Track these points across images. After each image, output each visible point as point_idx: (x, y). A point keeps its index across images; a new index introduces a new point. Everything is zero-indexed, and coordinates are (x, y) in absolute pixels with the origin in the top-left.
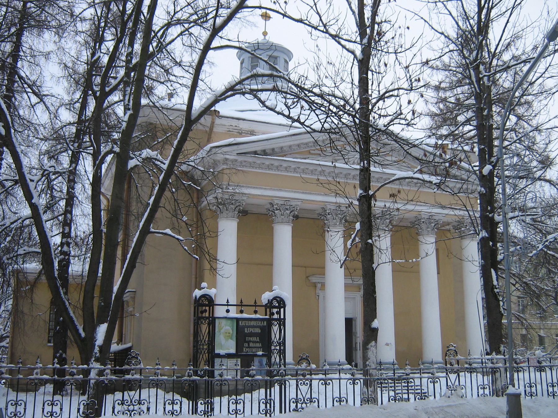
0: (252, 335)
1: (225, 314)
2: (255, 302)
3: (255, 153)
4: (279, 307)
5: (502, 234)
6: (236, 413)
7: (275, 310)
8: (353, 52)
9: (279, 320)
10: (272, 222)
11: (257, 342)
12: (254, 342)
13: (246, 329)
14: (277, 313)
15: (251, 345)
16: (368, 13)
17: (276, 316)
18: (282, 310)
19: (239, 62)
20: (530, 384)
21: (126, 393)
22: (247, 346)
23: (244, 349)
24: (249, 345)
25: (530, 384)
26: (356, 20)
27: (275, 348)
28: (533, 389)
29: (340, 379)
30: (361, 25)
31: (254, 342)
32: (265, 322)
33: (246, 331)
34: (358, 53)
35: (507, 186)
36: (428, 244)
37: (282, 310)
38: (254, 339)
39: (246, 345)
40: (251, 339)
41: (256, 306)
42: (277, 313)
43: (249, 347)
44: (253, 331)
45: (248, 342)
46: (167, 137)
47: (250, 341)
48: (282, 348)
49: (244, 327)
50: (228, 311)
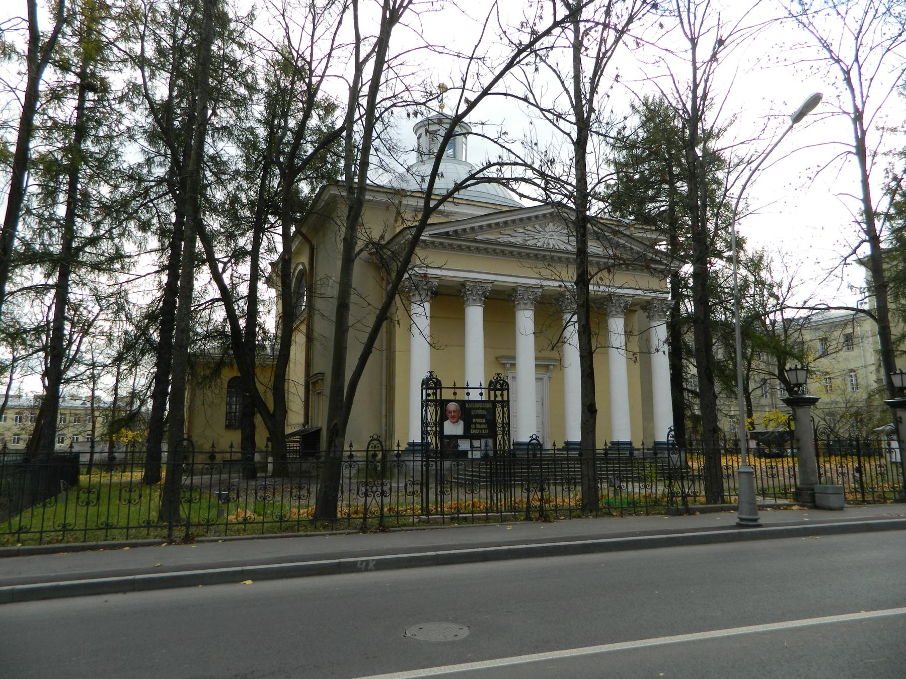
0: (478, 416)
4: (502, 390)
8: (569, 135)
9: (502, 402)
15: (478, 426)
16: (586, 86)
17: (430, 391)
20: (773, 477)
25: (773, 477)
26: (571, 102)
28: (730, 472)
34: (575, 135)
37: (438, 391)
38: (481, 420)
39: (473, 426)
40: (477, 420)
42: (433, 394)
43: (476, 428)
45: (475, 423)
46: (472, 513)
49: (470, 409)
50: (481, 394)
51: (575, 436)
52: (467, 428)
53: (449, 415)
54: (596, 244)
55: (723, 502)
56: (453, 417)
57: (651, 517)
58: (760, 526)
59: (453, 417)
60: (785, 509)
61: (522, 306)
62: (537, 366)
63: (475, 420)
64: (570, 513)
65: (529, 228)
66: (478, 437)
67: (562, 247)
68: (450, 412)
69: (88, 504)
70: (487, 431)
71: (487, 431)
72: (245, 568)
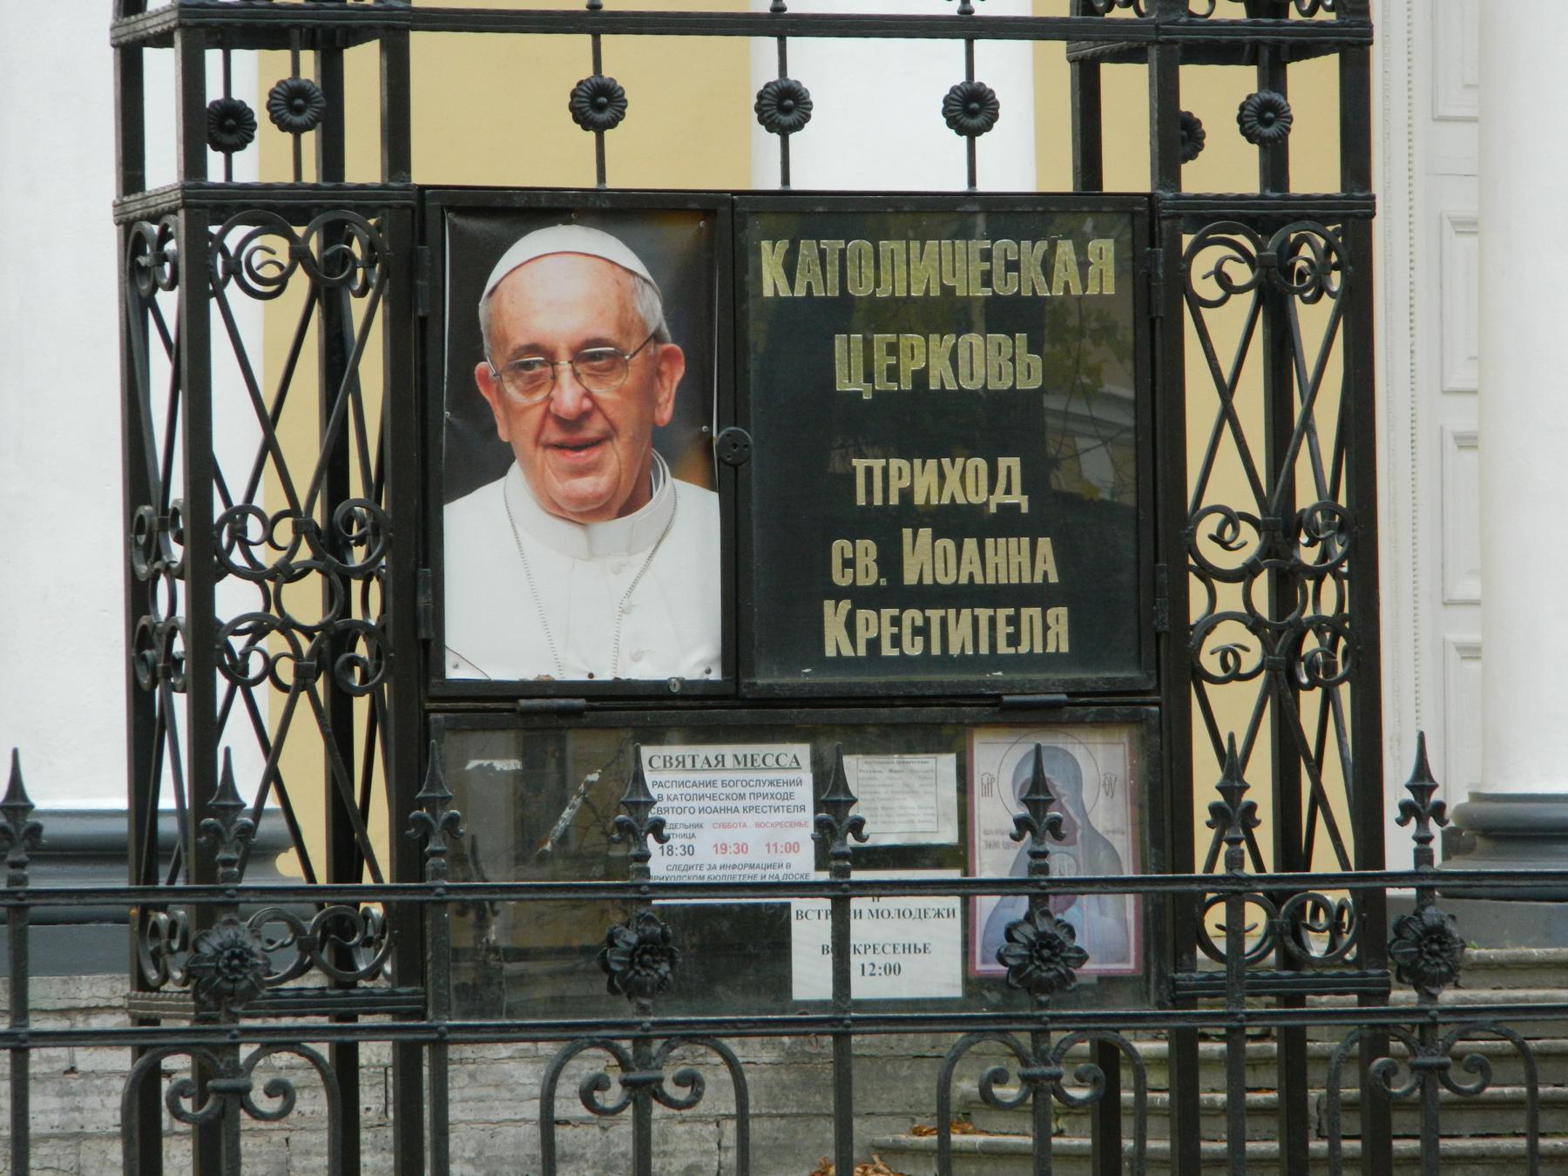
0: (931, 421)
1: (560, 159)
4: (1268, 47)
5: (386, 905)
7: (263, 160)
9: (1267, 216)
11: (1006, 523)
12: (956, 522)
13: (846, 350)
15: (924, 557)
18: (163, 167)
21: (970, 544)
22: (868, 574)
23: (834, 616)
24: (890, 561)
27: (1225, 618)
31: (956, 522)
32: (1104, 252)
33: (848, 381)
35: (1249, 1032)
37: (163, 167)
38: (961, 481)
39: (854, 561)
40: (926, 481)
43: (892, 592)
44: (940, 376)
45: (889, 525)
47: (908, 514)
52: (766, 589)
53: (517, 409)
59: (573, 435)
63: (885, 477)
68: (535, 360)
70: (1049, 631)
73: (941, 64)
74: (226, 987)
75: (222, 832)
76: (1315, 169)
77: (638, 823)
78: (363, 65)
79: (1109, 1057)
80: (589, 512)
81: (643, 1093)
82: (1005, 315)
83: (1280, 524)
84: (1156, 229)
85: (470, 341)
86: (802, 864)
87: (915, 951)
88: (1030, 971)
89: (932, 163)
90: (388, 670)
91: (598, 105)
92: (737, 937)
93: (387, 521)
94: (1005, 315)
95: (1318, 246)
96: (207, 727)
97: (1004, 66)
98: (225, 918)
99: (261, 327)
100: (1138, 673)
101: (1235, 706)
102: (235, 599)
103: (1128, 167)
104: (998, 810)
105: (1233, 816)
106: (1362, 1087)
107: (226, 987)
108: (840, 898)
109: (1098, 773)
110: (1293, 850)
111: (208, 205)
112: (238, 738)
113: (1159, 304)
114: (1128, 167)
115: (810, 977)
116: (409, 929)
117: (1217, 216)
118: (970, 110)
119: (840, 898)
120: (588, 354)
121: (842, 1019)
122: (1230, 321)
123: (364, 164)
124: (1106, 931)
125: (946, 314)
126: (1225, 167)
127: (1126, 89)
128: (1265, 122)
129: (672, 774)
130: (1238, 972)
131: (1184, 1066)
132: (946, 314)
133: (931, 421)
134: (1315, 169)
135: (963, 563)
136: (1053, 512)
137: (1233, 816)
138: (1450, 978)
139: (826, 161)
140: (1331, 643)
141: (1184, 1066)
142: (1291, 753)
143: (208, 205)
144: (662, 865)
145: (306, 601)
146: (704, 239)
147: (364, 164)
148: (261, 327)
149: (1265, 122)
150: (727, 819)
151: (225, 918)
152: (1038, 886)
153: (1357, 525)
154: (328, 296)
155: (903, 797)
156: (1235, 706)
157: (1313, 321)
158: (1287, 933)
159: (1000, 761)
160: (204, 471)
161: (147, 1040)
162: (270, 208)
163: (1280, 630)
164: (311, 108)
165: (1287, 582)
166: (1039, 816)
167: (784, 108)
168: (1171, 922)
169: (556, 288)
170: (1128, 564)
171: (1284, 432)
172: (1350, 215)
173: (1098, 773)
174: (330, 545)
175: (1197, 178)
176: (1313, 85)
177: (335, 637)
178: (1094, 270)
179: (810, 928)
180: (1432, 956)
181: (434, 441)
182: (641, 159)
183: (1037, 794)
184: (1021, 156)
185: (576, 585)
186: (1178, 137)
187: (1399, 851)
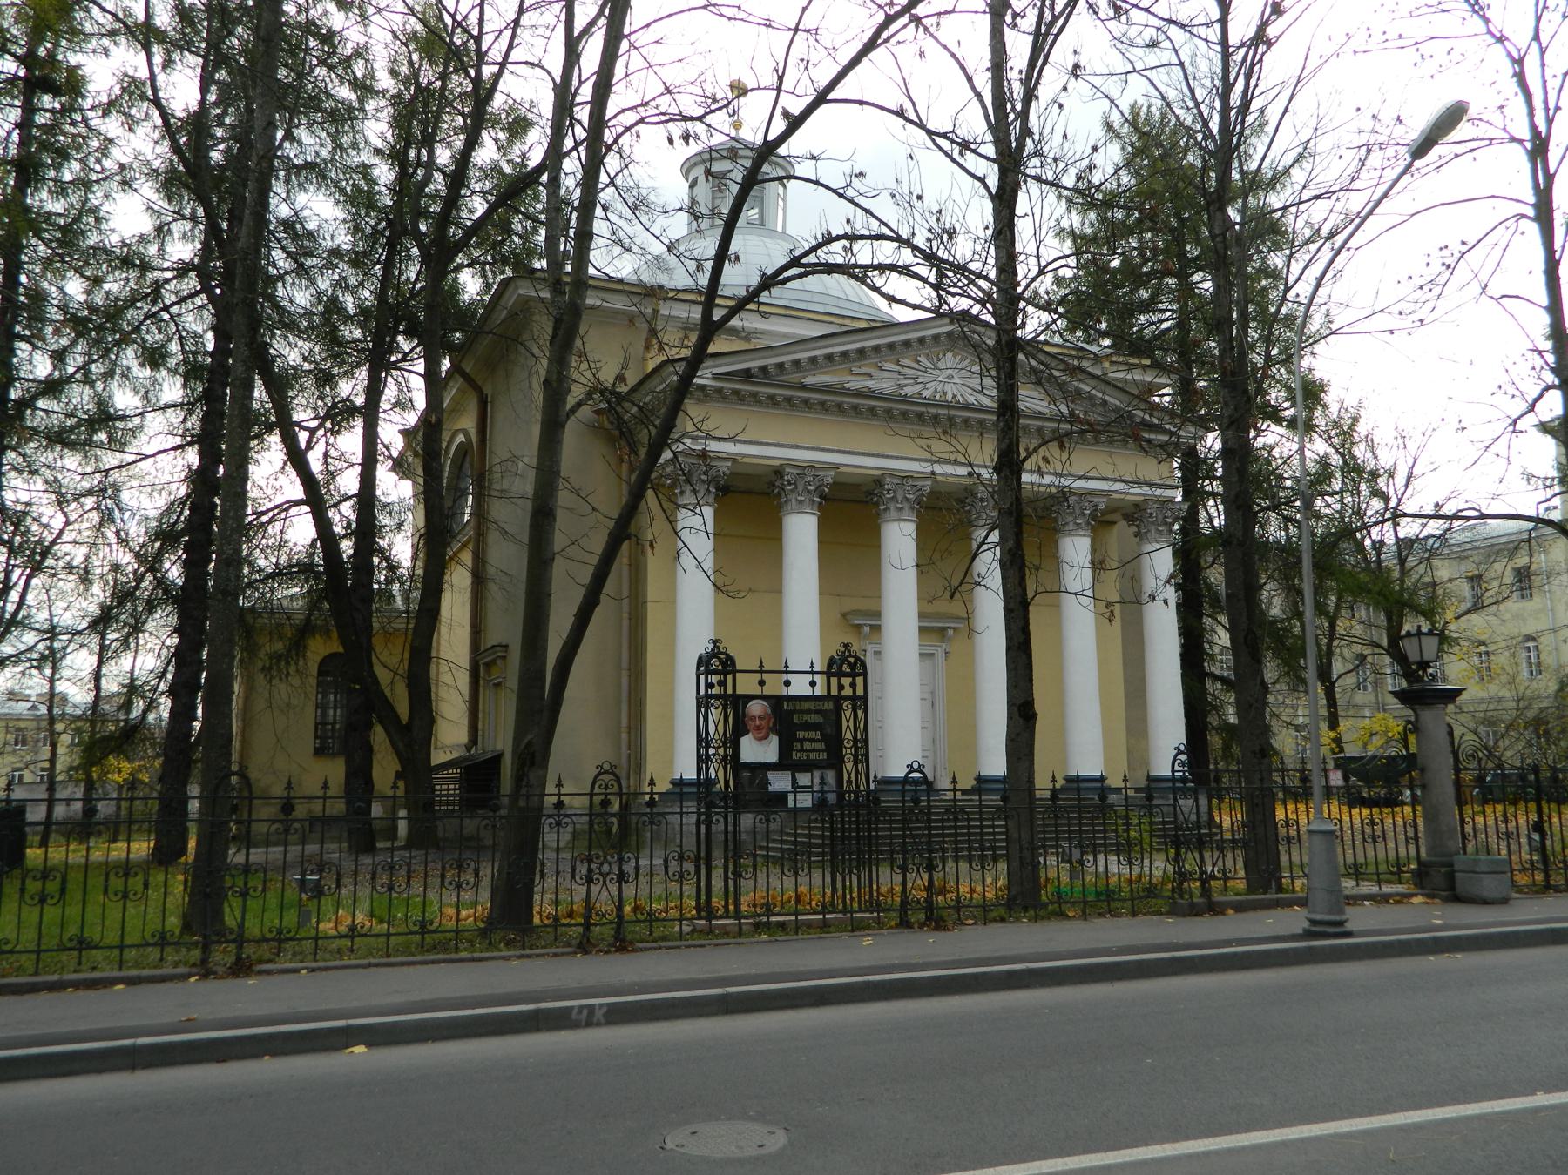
0: (808, 727)
1: (757, 690)
2: (761, 665)
3: (747, 373)
4: (854, 675)
6: (681, 876)
8: (982, 180)
9: (854, 698)
10: (780, 507)
12: (811, 740)
14: (720, 683)
15: (807, 745)
18: (702, 692)
19: (687, 185)
26: (987, 117)
27: (848, 753)
29: (681, 813)
30: (999, 127)
31: (811, 740)
34: (993, 182)
36: (900, 539)
37: (702, 692)
39: (797, 746)
40: (806, 735)
41: (761, 672)
43: (802, 750)
45: (801, 741)
48: (703, 751)
49: (791, 713)
51: (995, 765)
52: (784, 750)
53: (751, 725)
54: (1035, 394)
55: (1280, 889)
56: (758, 728)
57: (1139, 919)
58: (1349, 934)
59: (758, 728)
60: (1397, 902)
61: (893, 514)
62: (922, 630)
63: (801, 734)
64: (986, 913)
65: (906, 362)
66: (807, 767)
67: (971, 400)
68: (753, 718)
69: (42, 901)
70: (824, 756)
71: (824, 756)
72: (871, 978)
73: (809, 677)
74: (710, 805)
75: (709, 783)
76: (860, 692)
77: (766, 783)
78: (730, 677)
79: (832, 815)
80: (760, 739)
81: (768, 821)
82: (816, 712)
83: (855, 740)
84: (838, 700)
85: (744, 715)
86: (789, 788)
87: (805, 801)
88: (821, 804)
89: (808, 691)
90: (732, 760)
91: (762, 683)
92: (782, 797)
93: (732, 741)
94: (816, 712)
95: (860, 702)
96: (708, 769)
97: (817, 678)
98: (23, 706)
99: (715, 713)
100: (836, 762)
101: (849, 766)
102: (712, 751)
103: (834, 692)
104: (817, 781)
105: (849, 782)
106: (916, 786)
107: (710, 805)
108: (795, 793)
109: (830, 776)
110: (858, 786)
111: (708, 696)
112: (712, 770)
113: (838, 711)
114: (834, 692)
115: (791, 804)
116: (735, 797)
117: (846, 698)
118: (813, 684)
119: (795, 793)
120: (760, 717)
121: (796, 811)
122: (848, 713)
123: (730, 691)
124: (832, 798)
125: (809, 712)
126: (848, 692)
127: (834, 681)
128: (853, 685)
129: (771, 776)
130: (850, 803)
131: (843, 815)
132: (809, 712)
133: (808, 727)
134: (860, 692)
135: (813, 747)
136: (825, 738)
137: (849, 782)
138: (1117, 410)
139: (793, 691)
140: (862, 757)
141: (843, 815)
142: (857, 772)
143: (708, 696)
144: (770, 788)
145: (721, 751)
146: (776, 701)
147: (730, 691)
148: (715, 713)
149: (853, 685)
150: (779, 782)
151: (23, 706)
152: (822, 792)
153: (866, 741)
154: (725, 709)
155: (804, 779)
156: (849, 766)
157: (860, 713)
158: (857, 797)
159: (817, 774)
160: (707, 733)
161: (699, 814)
162: (716, 697)
163: (855, 756)
164: (722, 683)
165: (857, 749)
166: (823, 783)
167: (787, 683)
168: (841, 796)
169: (756, 708)
170: (834, 743)
171: (856, 729)
172: (865, 698)
173: (830, 776)
174: (725, 744)
175: (844, 693)
176: (860, 680)
177: (725, 756)
178: (830, 706)
179: (791, 797)
180: (877, 801)
181: (740, 728)
182: (767, 691)
183: (822, 778)
184: (818, 691)
185: (757, 750)
186: (841, 687)
187: (872, 787)
